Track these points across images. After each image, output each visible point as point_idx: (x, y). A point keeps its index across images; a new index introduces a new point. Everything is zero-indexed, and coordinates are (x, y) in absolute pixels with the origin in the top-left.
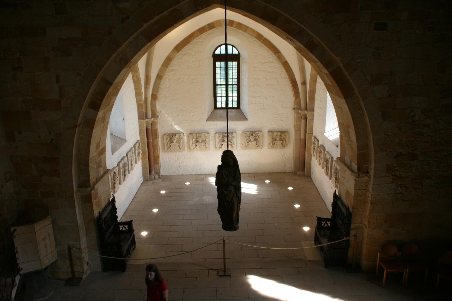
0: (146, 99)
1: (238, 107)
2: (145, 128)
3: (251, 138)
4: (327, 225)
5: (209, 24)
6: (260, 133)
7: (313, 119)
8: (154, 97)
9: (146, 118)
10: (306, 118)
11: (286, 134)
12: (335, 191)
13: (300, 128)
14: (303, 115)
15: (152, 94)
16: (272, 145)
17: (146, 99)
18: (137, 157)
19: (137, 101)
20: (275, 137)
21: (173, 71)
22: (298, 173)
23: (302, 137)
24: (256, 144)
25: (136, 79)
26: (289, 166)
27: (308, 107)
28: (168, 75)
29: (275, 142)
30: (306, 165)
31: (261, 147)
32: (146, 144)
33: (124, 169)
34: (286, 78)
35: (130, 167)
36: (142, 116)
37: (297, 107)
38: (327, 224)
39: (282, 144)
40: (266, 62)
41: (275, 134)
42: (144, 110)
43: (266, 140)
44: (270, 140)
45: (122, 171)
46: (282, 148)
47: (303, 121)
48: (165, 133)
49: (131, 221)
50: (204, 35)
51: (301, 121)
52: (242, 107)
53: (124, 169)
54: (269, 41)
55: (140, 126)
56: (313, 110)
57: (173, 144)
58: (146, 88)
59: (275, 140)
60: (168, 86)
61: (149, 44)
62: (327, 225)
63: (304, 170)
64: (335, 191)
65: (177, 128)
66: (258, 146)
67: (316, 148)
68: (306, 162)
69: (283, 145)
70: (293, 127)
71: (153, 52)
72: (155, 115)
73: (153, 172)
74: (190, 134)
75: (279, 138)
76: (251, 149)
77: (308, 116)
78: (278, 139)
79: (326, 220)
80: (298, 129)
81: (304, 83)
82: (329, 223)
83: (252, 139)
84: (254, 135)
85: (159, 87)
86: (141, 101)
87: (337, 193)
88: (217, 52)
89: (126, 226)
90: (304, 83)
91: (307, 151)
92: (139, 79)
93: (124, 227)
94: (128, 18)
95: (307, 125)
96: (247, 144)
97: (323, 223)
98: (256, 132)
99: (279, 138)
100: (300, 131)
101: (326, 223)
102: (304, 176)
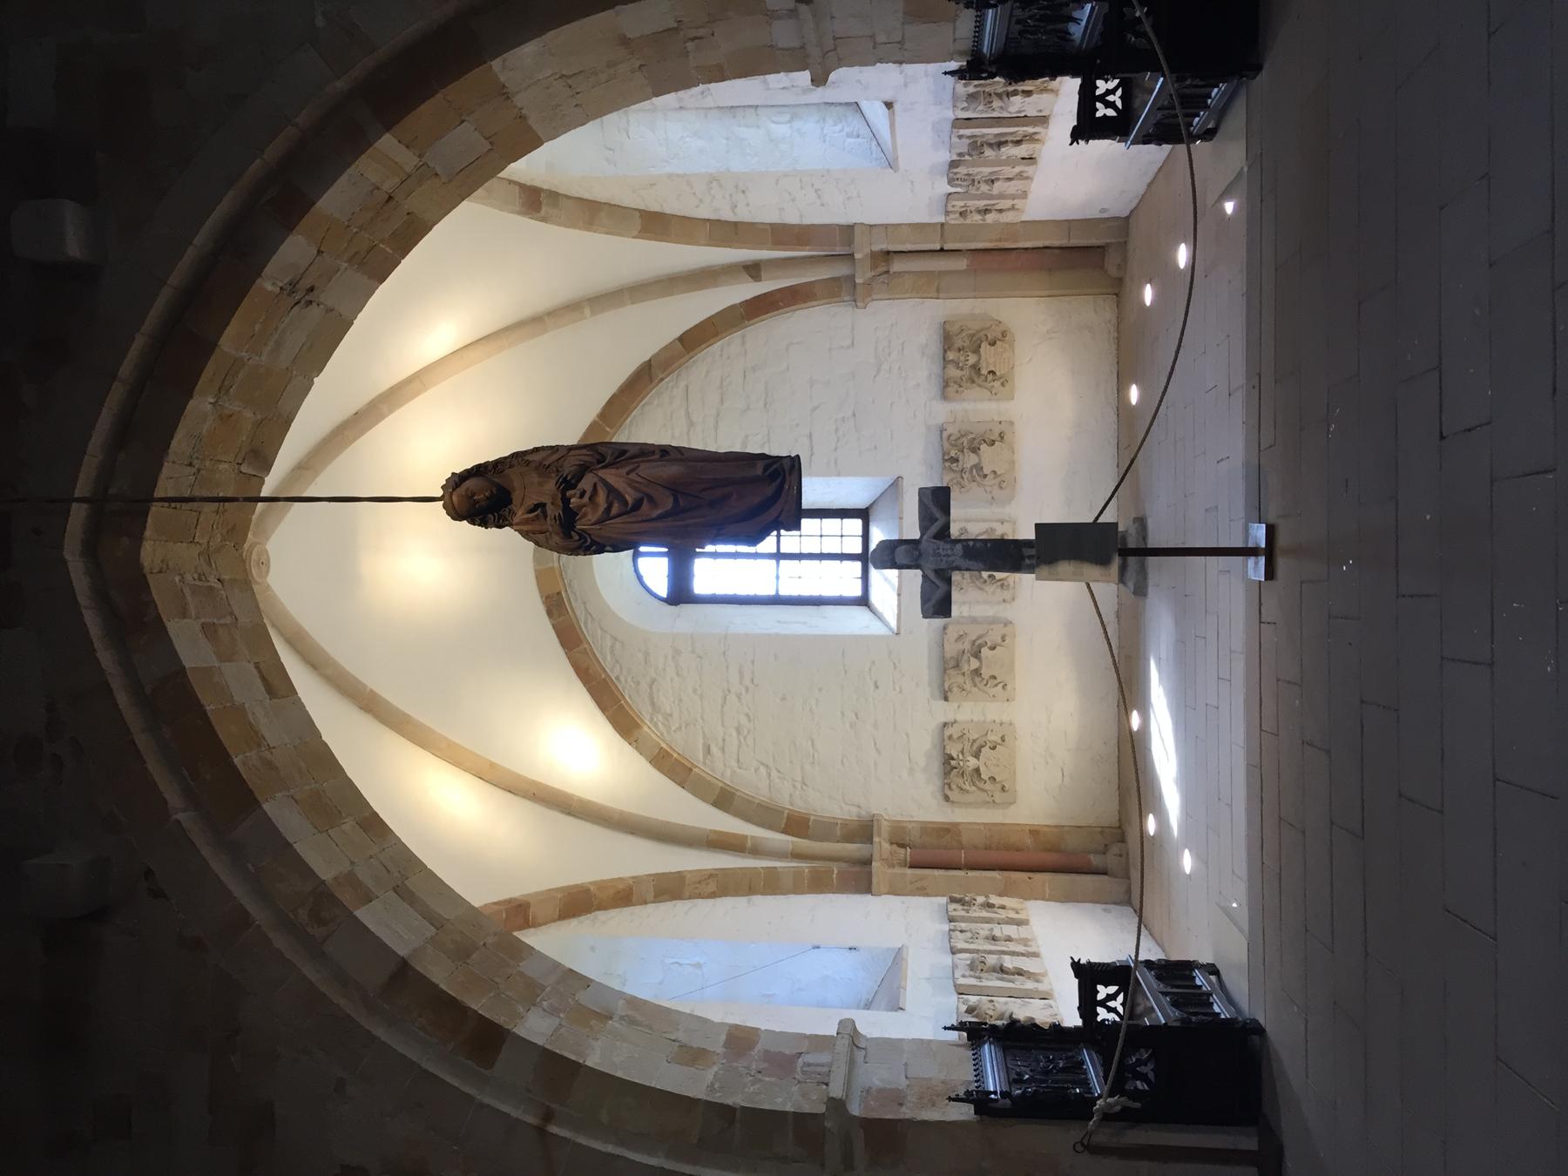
0: (797, 855)
1: (864, 514)
2: (909, 871)
3: (968, 465)
4: (1113, 92)
5: (550, 613)
6: (950, 430)
7: (886, 226)
8: (796, 825)
9: (867, 862)
10: (888, 254)
11: (955, 329)
12: (952, 73)
13: (929, 274)
14: (874, 267)
15: (785, 831)
16: (997, 384)
17: (797, 855)
18: (1003, 914)
19: (797, 890)
20: (966, 372)
21: (708, 750)
22: (1112, 270)
23: (961, 264)
24: (993, 443)
25: (712, 887)
26: (1091, 311)
27: (839, 250)
28: (722, 769)
29: (984, 372)
30: (1074, 242)
31: (1003, 427)
32: (972, 874)
33: (993, 970)
34: (743, 337)
35: (1012, 947)
36: (858, 878)
37: (842, 290)
38: (1109, 92)
39: (993, 344)
40: (688, 414)
41: (953, 372)
42: (835, 868)
43: (977, 408)
44: (976, 391)
45: (993, 982)
46: (1012, 346)
47: (898, 266)
48: (940, 797)
49: (1077, 968)
50: (589, 631)
51: (899, 274)
52: (859, 502)
53: (993, 970)
54: (610, 402)
55: (895, 891)
56: (848, 231)
57: (982, 769)
58: (756, 850)
59: (976, 368)
60: (763, 770)
61: (281, 811)
62: (1113, 92)
63: (1101, 249)
64: (952, 73)
65: (923, 744)
66: (1001, 436)
67: (981, 204)
68: (1064, 242)
69: (999, 337)
70: (931, 303)
71: (622, 813)
72: (864, 831)
73: (1096, 860)
74: (946, 699)
75: (967, 358)
76: (1013, 463)
77: (876, 248)
78: (972, 359)
79: (1087, 99)
80: (932, 286)
81: (753, 270)
82: (1102, 86)
83: (970, 460)
84: (953, 454)
85: (760, 805)
86: (798, 874)
87: (953, 65)
88: (662, 589)
89: (1103, 992)
90: (753, 270)
91: (1016, 241)
92: (712, 875)
93: (1103, 1004)
94: (149, 873)
95: (909, 247)
96: (989, 481)
97: (1102, 111)
98: (946, 445)
99: (967, 358)
100: (941, 274)
101: (1102, 98)
102: (945, 670)
